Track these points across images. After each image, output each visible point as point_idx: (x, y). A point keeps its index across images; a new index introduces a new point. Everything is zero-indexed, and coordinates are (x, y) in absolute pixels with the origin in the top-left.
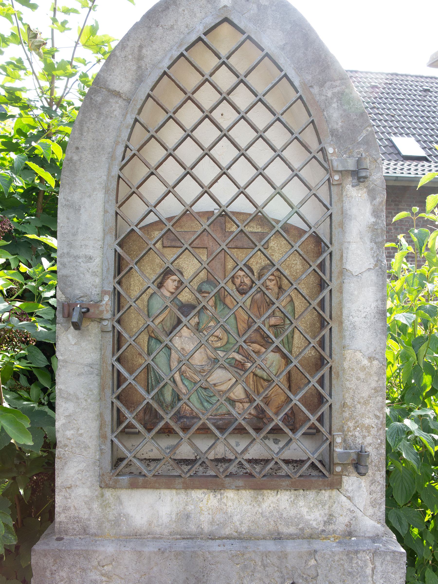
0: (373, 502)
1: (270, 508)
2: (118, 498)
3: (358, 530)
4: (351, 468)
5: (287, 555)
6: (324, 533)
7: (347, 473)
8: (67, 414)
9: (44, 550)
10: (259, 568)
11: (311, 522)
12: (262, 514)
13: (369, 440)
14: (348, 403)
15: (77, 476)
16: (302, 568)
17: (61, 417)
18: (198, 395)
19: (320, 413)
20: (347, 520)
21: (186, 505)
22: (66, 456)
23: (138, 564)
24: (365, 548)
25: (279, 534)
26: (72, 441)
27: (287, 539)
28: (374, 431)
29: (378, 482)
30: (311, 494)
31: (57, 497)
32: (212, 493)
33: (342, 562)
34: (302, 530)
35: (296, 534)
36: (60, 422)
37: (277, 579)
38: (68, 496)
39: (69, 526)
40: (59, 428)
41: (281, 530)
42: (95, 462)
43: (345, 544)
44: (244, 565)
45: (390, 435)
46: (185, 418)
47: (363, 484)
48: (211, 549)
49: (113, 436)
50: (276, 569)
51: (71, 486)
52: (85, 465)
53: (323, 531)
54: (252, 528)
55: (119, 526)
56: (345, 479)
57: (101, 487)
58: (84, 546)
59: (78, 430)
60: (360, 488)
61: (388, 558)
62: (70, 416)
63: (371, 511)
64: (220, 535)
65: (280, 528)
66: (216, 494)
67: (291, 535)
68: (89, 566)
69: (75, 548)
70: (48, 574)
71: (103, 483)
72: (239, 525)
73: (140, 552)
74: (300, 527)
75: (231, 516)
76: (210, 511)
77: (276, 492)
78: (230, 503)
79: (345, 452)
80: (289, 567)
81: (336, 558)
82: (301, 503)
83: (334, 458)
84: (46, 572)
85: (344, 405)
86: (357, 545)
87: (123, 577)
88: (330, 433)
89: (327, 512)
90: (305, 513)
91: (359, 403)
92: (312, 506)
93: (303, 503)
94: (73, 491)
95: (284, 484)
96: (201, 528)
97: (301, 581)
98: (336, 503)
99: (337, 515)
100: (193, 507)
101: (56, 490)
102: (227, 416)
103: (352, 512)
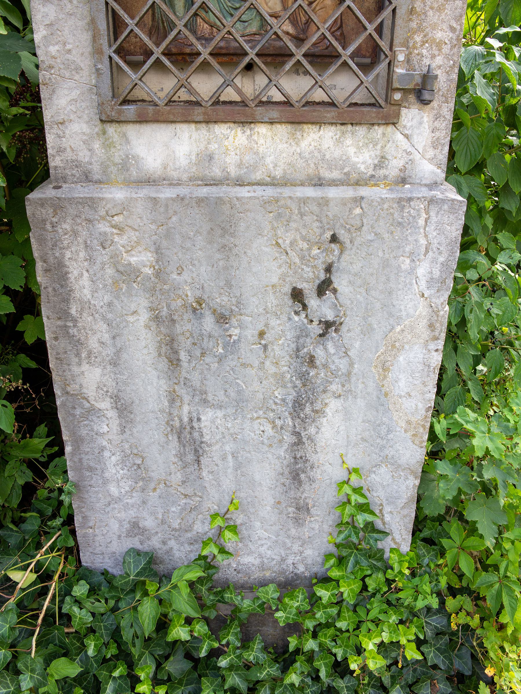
0: (435, 143)
1: (311, 147)
2: (124, 135)
3: (414, 176)
4: (412, 98)
5: (328, 201)
6: (373, 179)
7: (407, 105)
8: (48, 23)
9: (40, 199)
10: (295, 217)
11: (358, 166)
12: (300, 154)
13: (439, 60)
14: (417, 9)
15: (70, 107)
16: (345, 217)
17: (40, 26)
18: (219, 6)
19: (379, 20)
20: (400, 163)
21: (208, 143)
22: (53, 80)
23: (154, 213)
24: (420, 196)
25: (320, 179)
26: (58, 61)
27: (329, 185)
28: (446, 49)
29: (444, 117)
30: (361, 131)
31: (47, 135)
32: (240, 128)
33: (392, 211)
34: (347, 174)
35: (339, 180)
36: (39, 33)
37: (316, 230)
38: (62, 135)
39: (67, 171)
40: (39, 43)
41: (322, 175)
42: (91, 89)
43: (397, 191)
44: (278, 213)
45: (465, 61)
46: (203, 39)
47: (425, 119)
48: (239, 195)
49: (111, 51)
50: (315, 218)
51: (64, 121)
52: (78, 93)
53: (373, 176)
54: (289, 172)
55: (128, 170)
56: (404, 111)
57: (101, 120)
58: (88, 193)
59: (64, 44)
60: (421, 123)
61: (446, 207)
62: (51, 25)
63: (431, 153)
64: (250, 181)
65: (321, 171)
66: (245, 129)
67: (334, 181)
68: (96, 217)
69: (77, 195)
70: (49, 227)
71: (103, 115)
72: (272, 169)
73: (155, 198)
74: (345, 171)
75: (263, 157)
76: (238, 150)
77: (318, 127)
78: (261, 141)
79: (407, 74)
80: (331, 216)
81: (386, 206)
82: (348, 142)
83: (394, 81)
84: (45, 224)
85: (412, 11)
86: (411, 192)
87: (137, 228)
88: (391, 49)
89: (378, 153)
90: (352, 154)
91: (432, 8)
92: (361, 145)
93: (351, 142)
94: (66, 127)
95: (329, 115)
96: (227, 172)
97: (343, 232)
98: (391, 142)
99: (390, 158)
100: (216, 146)
101: (46, 127)
102: (258, 36)
103: (409, 153)
